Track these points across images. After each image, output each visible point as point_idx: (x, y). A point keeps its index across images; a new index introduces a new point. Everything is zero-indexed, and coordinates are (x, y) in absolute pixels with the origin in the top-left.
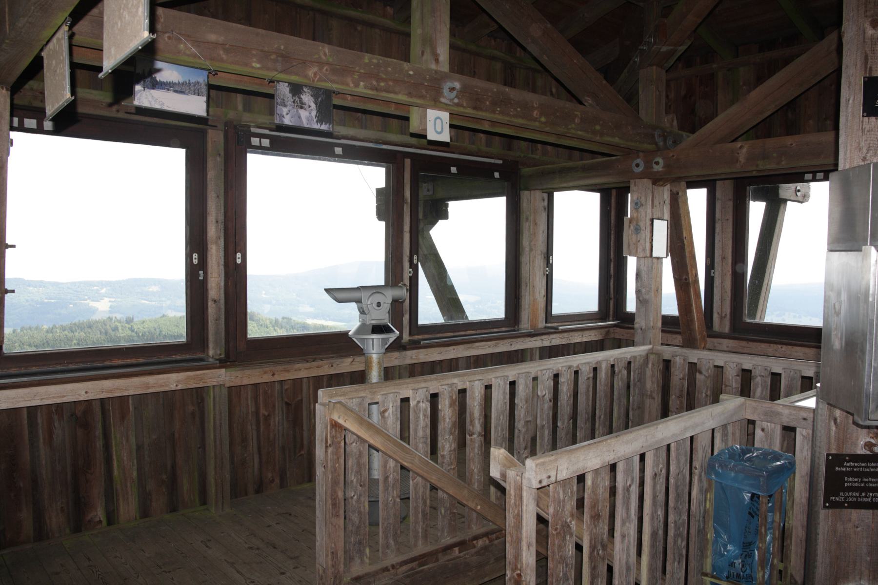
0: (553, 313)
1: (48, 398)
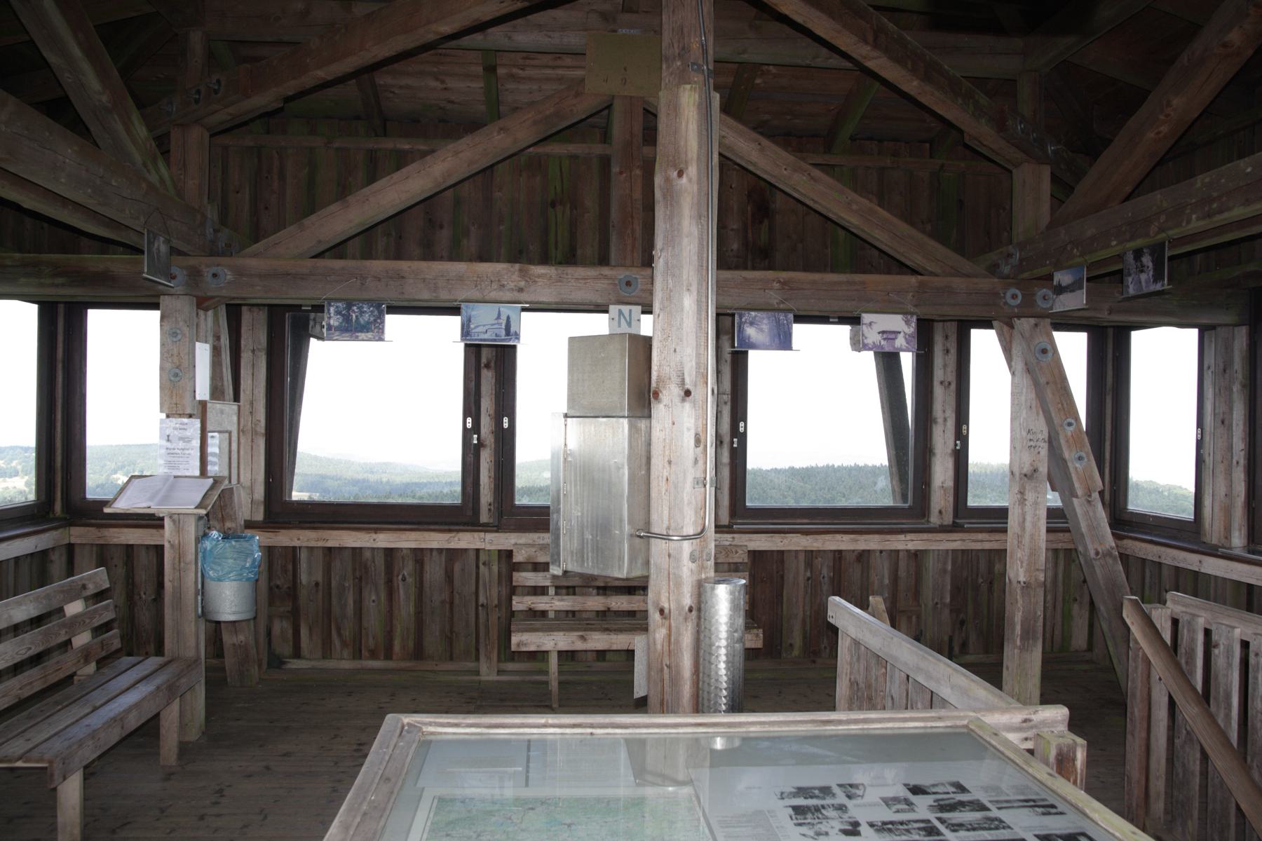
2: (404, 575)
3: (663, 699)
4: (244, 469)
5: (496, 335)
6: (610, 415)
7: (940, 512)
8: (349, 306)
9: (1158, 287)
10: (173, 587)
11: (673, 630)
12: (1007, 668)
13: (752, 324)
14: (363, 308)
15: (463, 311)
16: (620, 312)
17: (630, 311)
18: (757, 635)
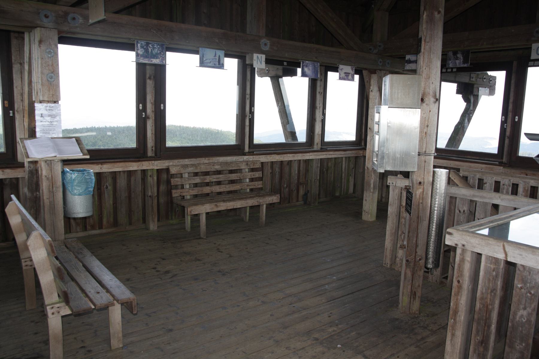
0: (325, 140)
1: (439, 164)
2: (107, 185)
3: (419, 216)
4: (20, 133)
6: (412, 107)
7: (317, 144)
8: (148, 44)
9: (465, 65)
10: (50, 202)
11: (425, 189)
12: (366, 200)
13: (306, 66)
14: (154, 45)
15: (200, 52)
16: (258, 57)
17: (261, 57)
18: (278, 197)
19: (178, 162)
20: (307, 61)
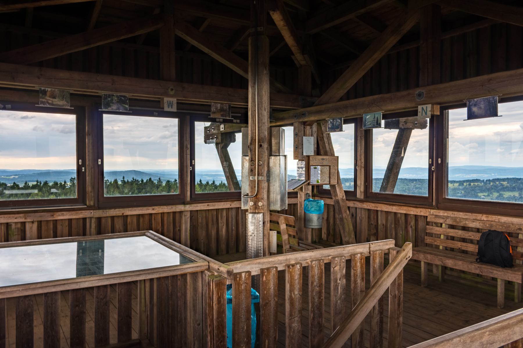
2: (411, 225)
5: (374, 125)
13: (475, 105)
16: (423, 108)
17: (427, 107)
19: (452, 214)
20: (475, 98)
